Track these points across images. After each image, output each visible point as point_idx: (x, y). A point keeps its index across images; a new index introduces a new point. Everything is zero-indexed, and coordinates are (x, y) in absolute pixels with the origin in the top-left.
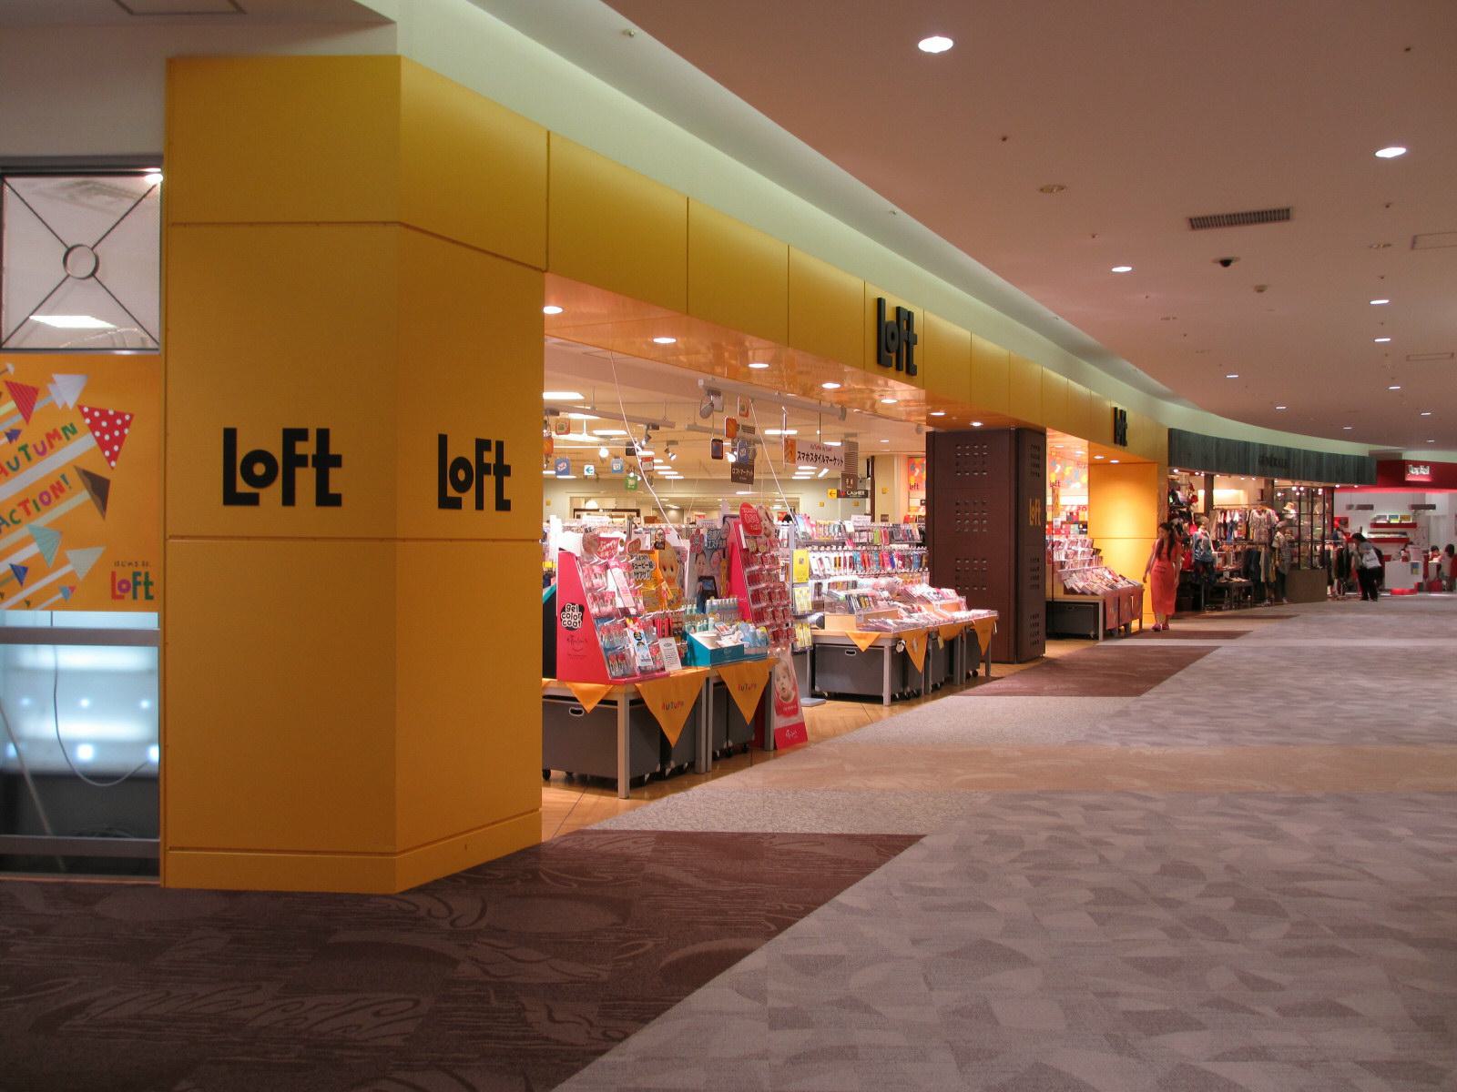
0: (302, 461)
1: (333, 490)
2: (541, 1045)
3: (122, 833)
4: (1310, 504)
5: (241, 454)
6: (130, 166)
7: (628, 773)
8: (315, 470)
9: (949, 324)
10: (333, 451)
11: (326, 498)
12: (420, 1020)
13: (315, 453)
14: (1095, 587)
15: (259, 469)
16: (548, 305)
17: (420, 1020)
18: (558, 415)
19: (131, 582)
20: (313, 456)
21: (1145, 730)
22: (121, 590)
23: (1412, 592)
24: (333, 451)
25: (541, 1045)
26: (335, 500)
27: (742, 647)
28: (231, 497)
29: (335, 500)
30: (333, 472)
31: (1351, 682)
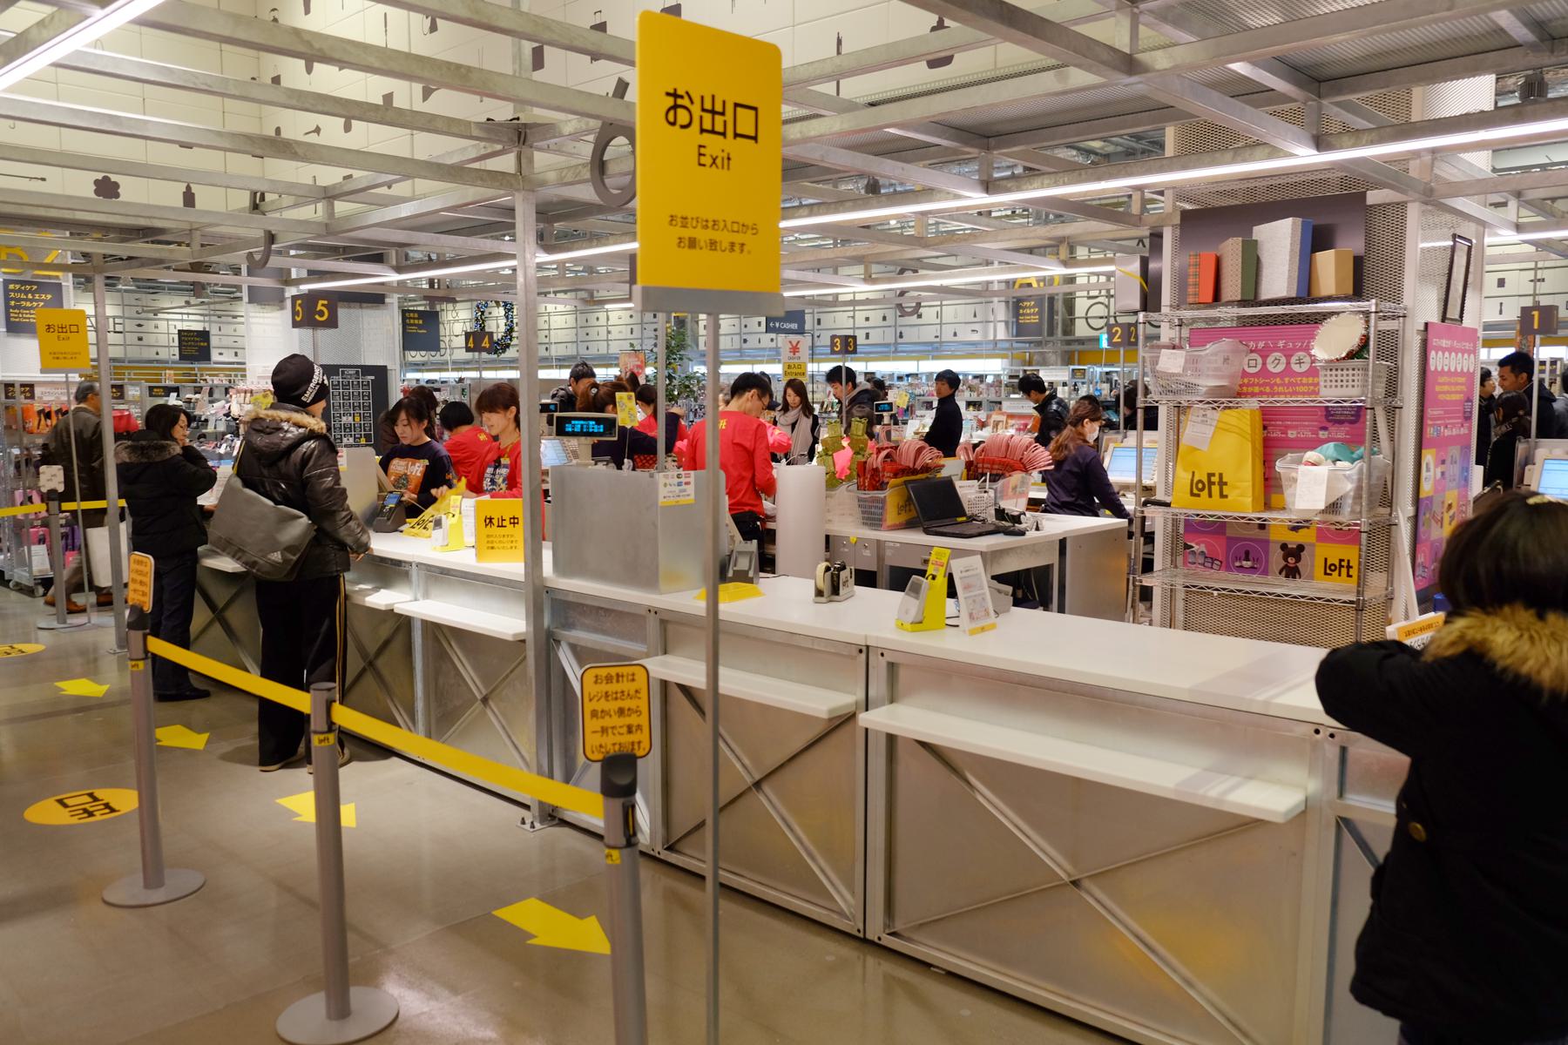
0: (1214, 483)
3: (810, 276)
5: (1328, 564)
6: (1515, 92)
10: (1224, 480)
11: (1222, 496)
15: (1200, 486)
16: (824, 719)
18: (1478, 463)
21: (1500, 524)
22: (1197, 488)
24: (1224, 480)
26: (1226, 496)
28: (1326, 574)
29: (1226, 496)
31: (389, 701)
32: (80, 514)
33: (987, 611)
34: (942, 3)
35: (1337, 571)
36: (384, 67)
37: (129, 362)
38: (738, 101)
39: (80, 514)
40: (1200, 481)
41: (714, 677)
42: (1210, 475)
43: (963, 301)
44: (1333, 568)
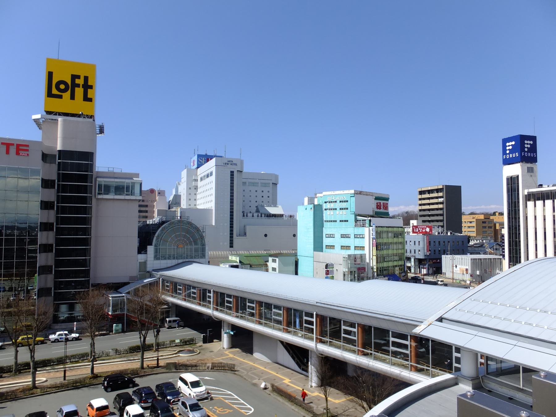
0: (78, 86)
1: (89, 96)
2: (437, 198)
4: (387, 234)
7: (256, 331)
8: (83, 89)
9: (28, 370)
10: (90, 84)
11: (87, 99)
12: (362, 401)
13: (83, 83)
14: (350, 375)
17: (362, 401)
19: (69, 83)
20: (82, 85)
23: (468, 215)
24: (90, 84)
25: (437, 198)
27: (205, 341)
29: (90, 100)
30: (89, 90)
32: (550, 198)
33: (161, 249)
34: (211, 416)
35: (69, 92)
36: (127, 360)
37: (510, 208)
38: (327, 245)
39: (550, 198)
40: (59, 83)
41: (453, 281)
42: (74, 77)
43: (399, 370)
44: (62, 87)
